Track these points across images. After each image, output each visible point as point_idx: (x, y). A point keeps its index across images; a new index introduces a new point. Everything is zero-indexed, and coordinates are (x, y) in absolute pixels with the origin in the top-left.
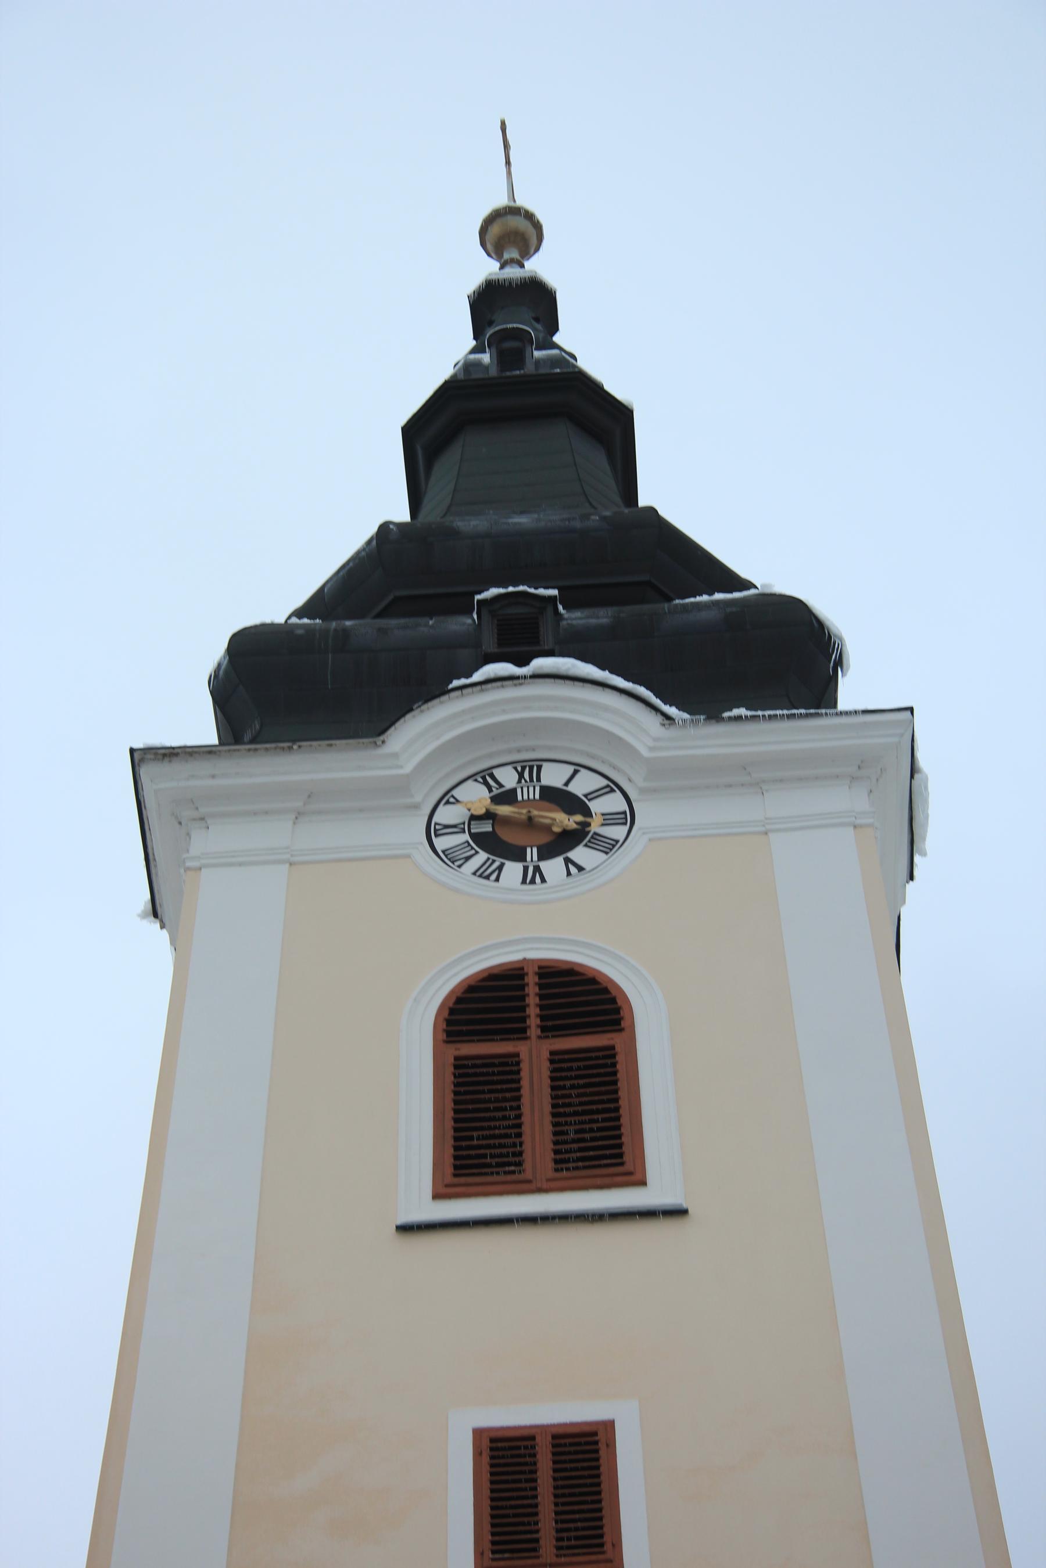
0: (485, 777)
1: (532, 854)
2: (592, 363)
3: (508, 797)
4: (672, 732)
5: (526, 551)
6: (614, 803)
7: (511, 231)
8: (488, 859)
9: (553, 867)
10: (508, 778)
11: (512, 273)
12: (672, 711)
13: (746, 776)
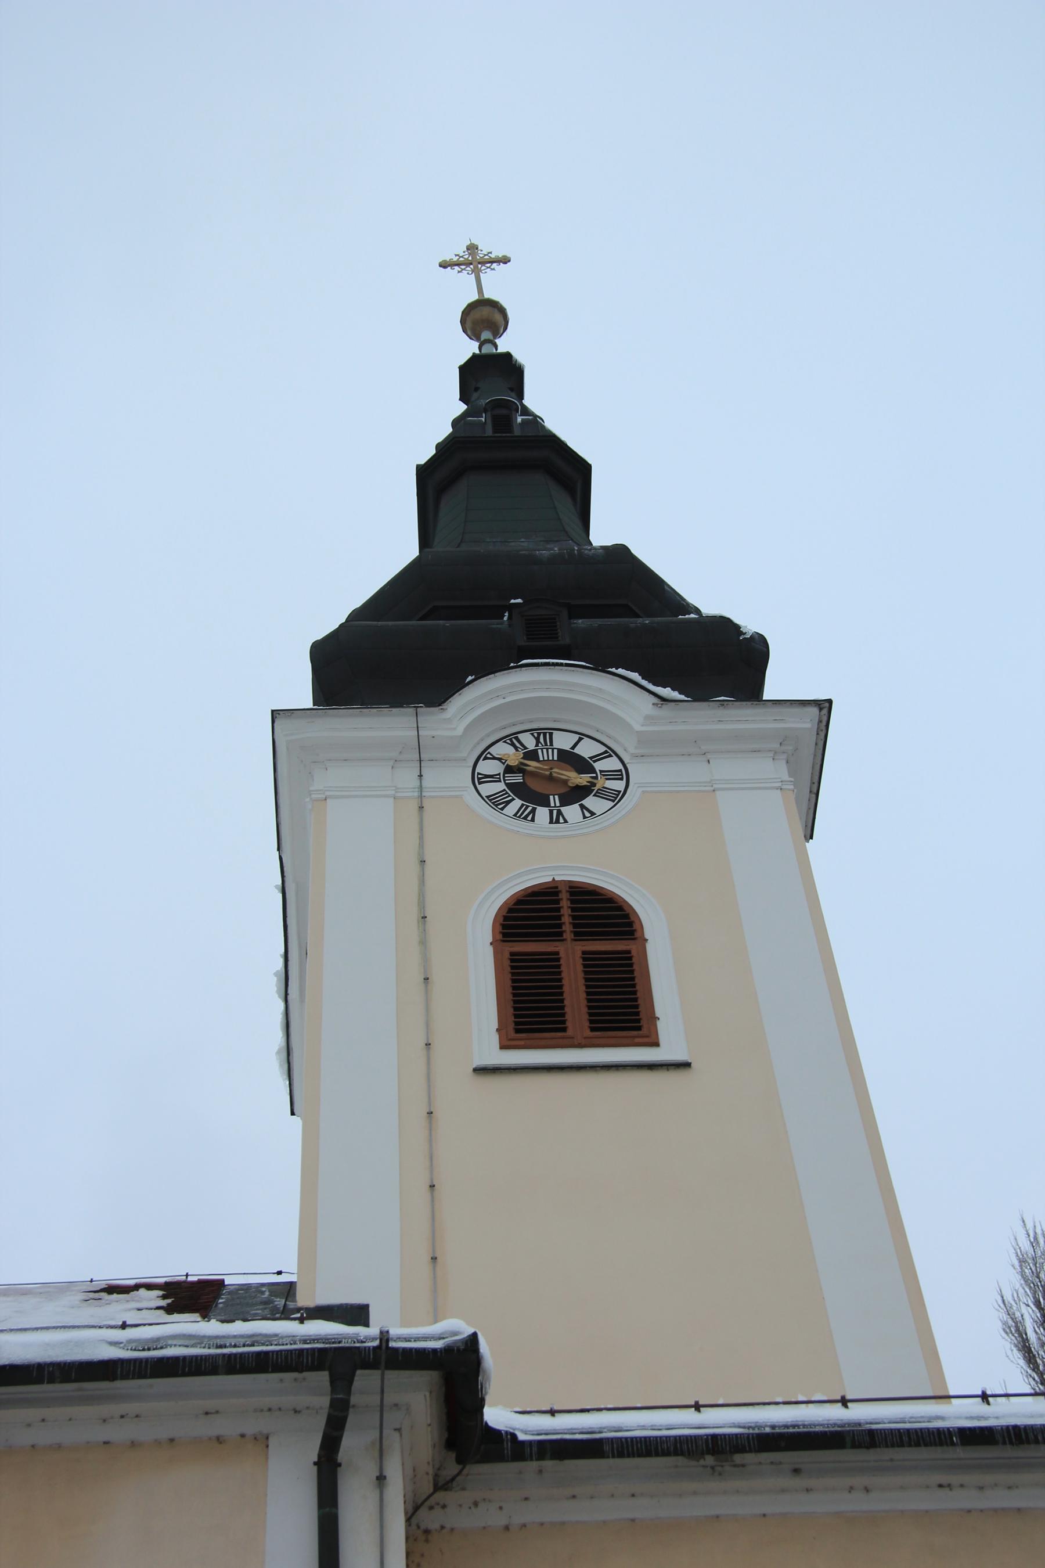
0: (513, 739)
1: (554, 800)
2: (556, 424)
3: (532, 755)
4: (666, 711)
5: (510, 577)
6: (611, 764)
7: (484, 318)
8: (523, 805)
9: (572, 812)
10: (529, 742)
11: (488, 349)
12: (666, 692)
13: (700, 749)
